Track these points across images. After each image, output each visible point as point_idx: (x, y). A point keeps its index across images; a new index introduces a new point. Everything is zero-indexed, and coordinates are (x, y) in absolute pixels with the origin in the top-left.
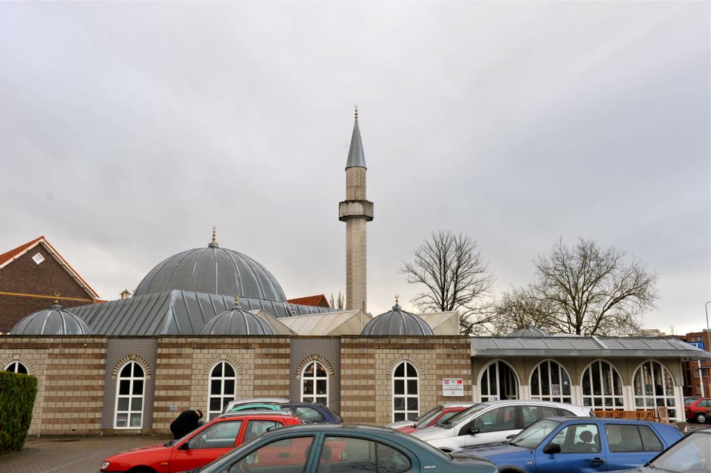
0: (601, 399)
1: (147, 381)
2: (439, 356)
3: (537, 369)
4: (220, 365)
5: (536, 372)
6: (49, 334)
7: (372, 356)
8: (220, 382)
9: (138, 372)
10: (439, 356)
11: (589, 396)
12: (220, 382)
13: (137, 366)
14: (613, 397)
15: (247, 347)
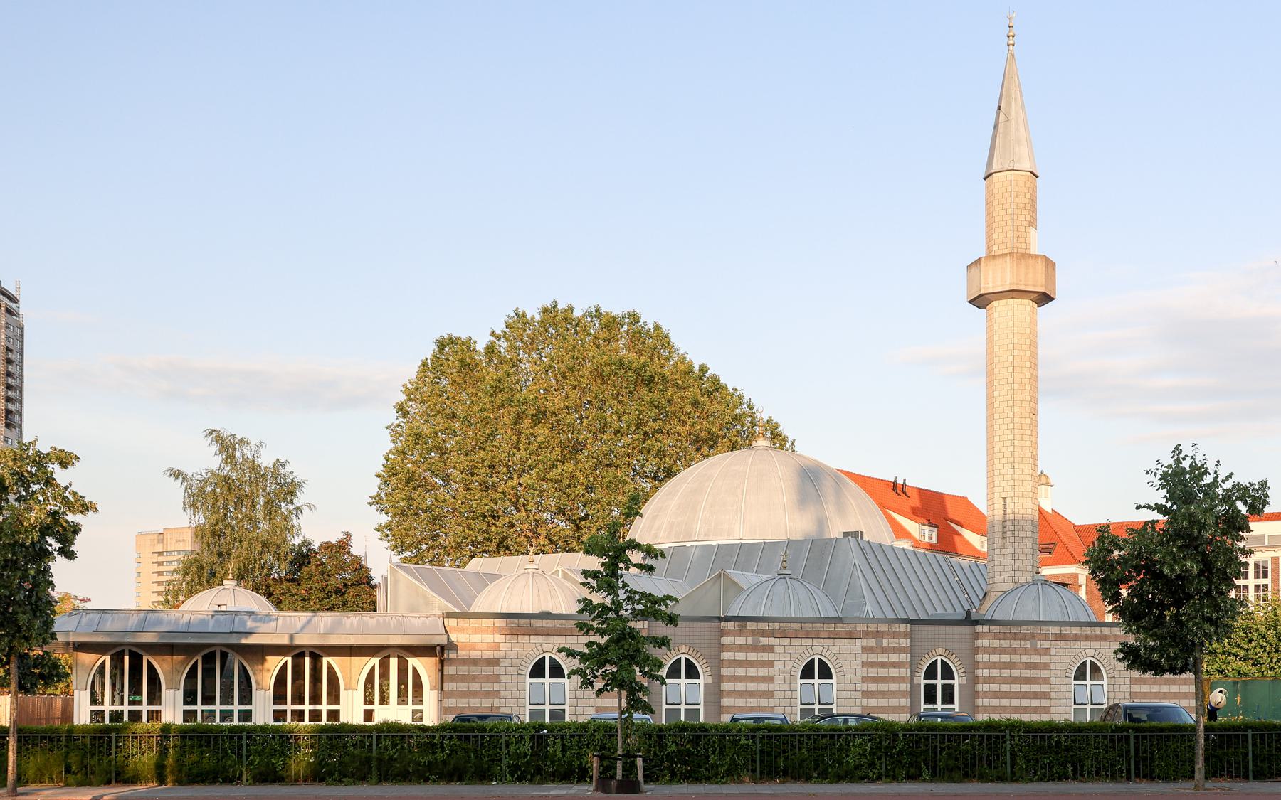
0: (320, 711)
1: (706, 685)
2: (866, 649)
3: (196, 663)
4: (1084, 664)
5: (193, 670)
6: (518, 611)
7: (770, 649)
8: (934, 686)
9: (948, 673)
10: (866, 649)
11: (229, 707)
12: (934, 686)
13: (690, 665)
14: (145, 708)
15: (851, 636)
